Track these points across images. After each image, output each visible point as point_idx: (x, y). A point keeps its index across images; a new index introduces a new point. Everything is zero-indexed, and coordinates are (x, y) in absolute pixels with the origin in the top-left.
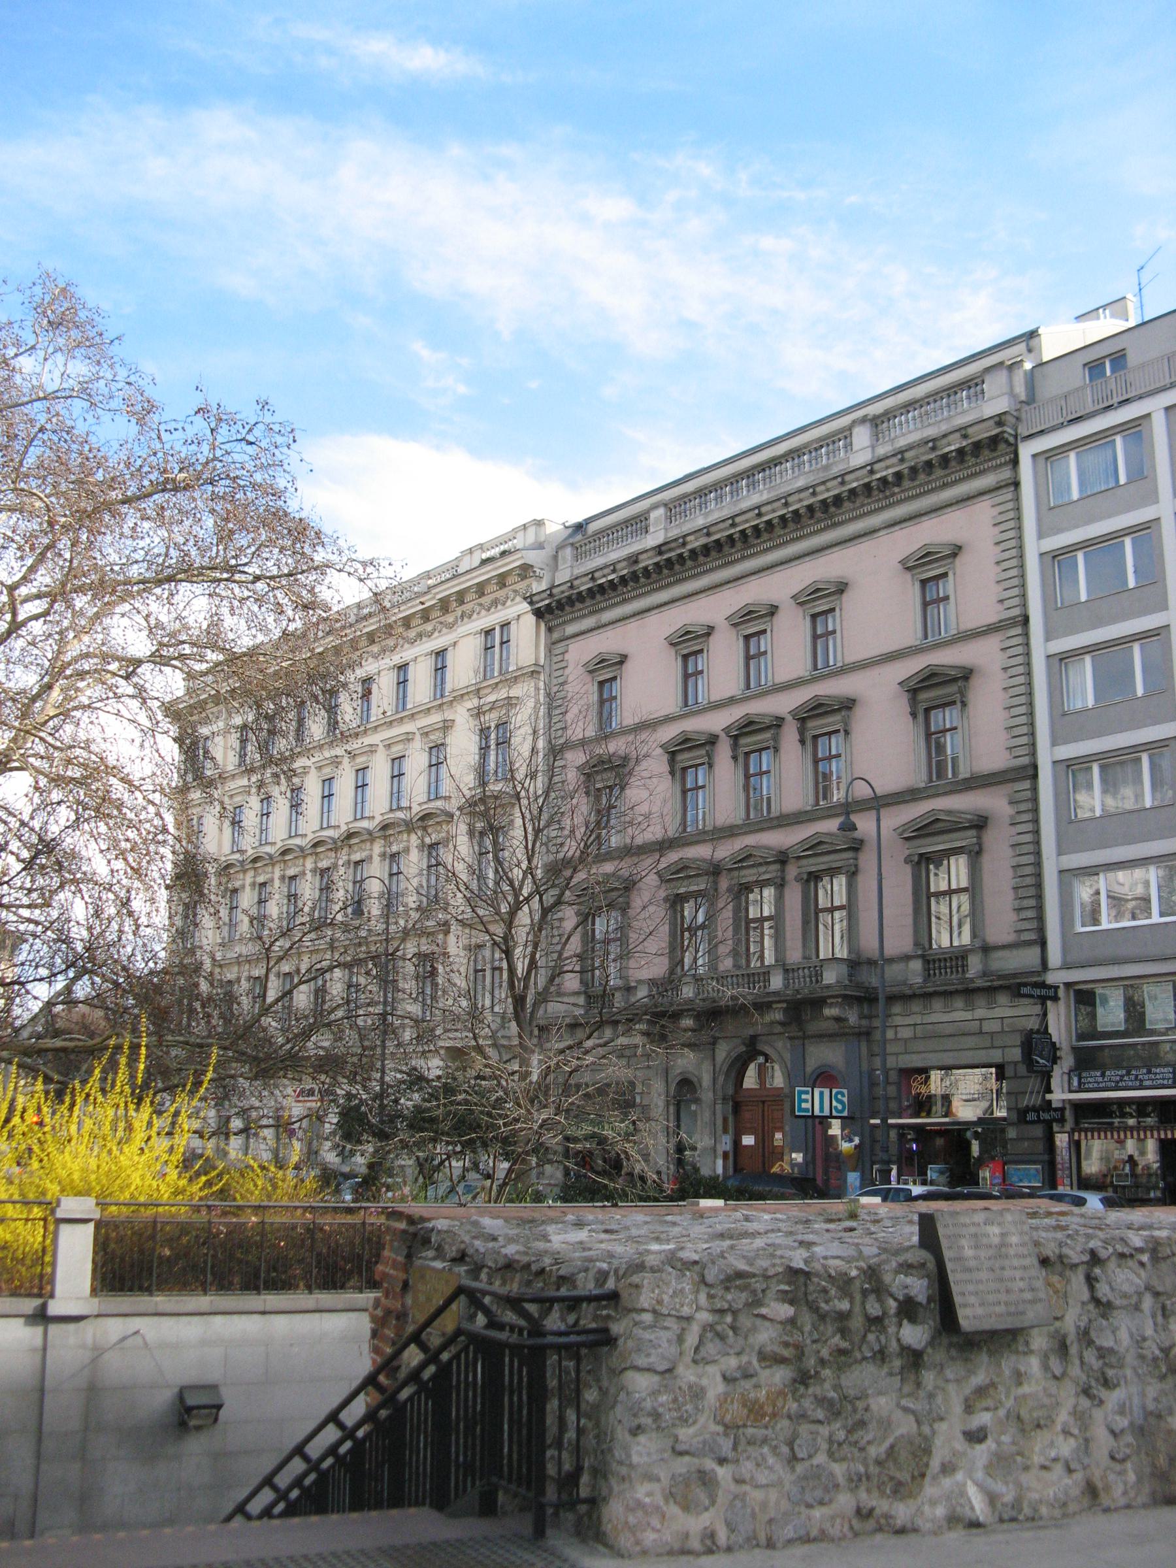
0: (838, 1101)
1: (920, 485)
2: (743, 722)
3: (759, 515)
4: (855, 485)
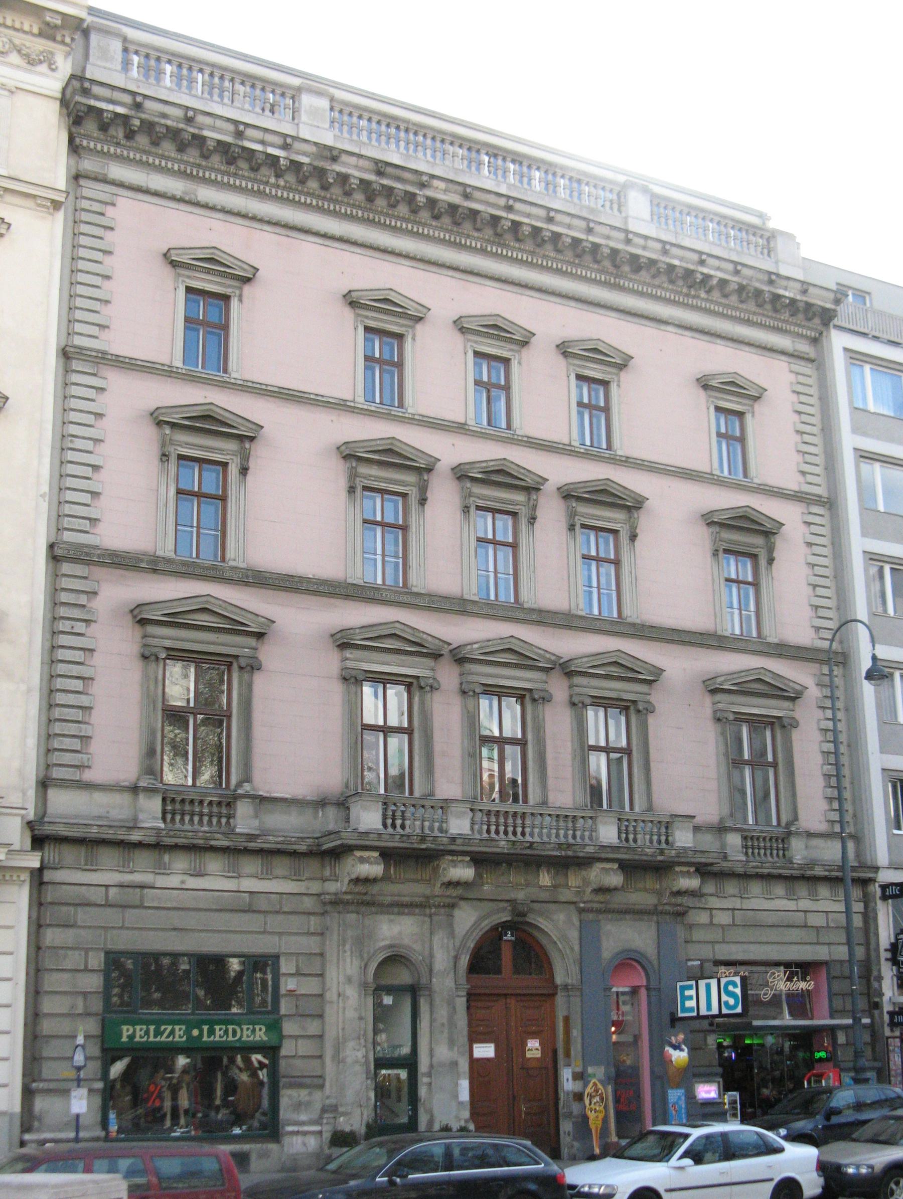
1: (746, 311)
2: (493, 466)
3: (550, 220)
4: (676, 262)
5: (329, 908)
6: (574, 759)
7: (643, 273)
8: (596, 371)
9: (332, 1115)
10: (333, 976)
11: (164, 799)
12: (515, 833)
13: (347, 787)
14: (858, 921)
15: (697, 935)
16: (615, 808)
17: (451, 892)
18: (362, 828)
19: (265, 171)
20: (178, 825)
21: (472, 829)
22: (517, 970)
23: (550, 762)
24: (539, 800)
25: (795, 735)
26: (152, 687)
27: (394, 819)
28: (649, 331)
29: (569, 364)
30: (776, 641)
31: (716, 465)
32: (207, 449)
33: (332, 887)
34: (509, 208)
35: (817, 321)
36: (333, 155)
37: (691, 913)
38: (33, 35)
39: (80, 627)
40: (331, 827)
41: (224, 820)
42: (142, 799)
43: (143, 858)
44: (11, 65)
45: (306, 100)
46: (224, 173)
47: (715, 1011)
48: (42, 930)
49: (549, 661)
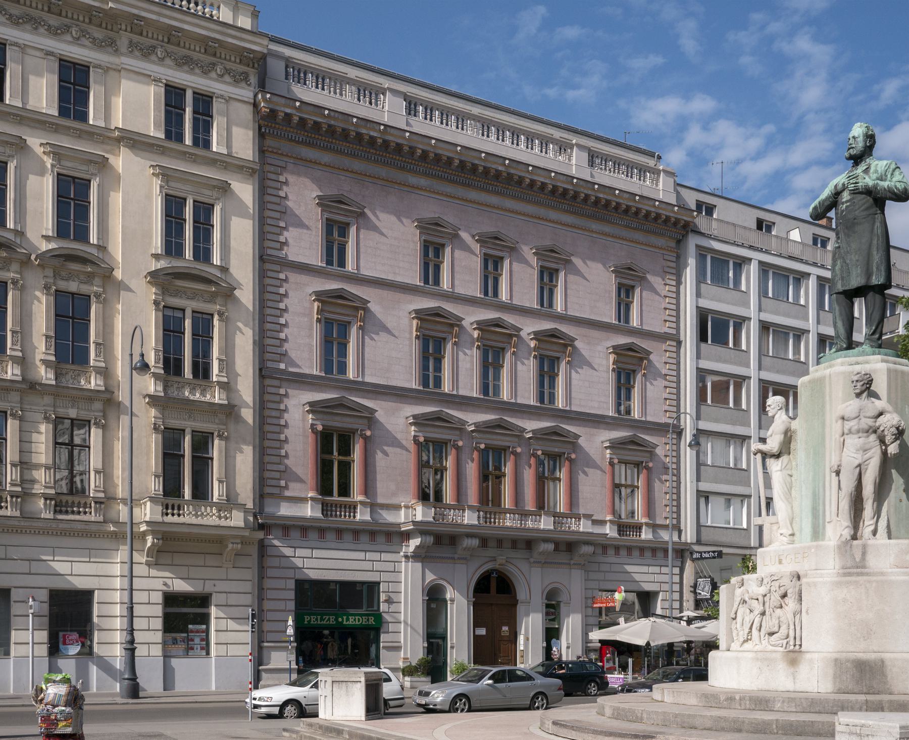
9: (151, 359)
22: (340, 495)
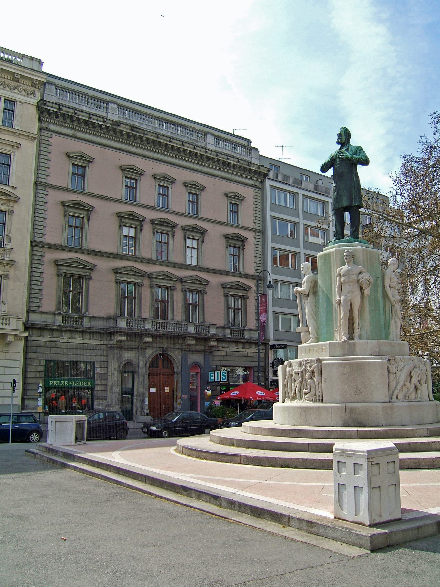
0: (223, 375)
1: (235, 171)
3: (183, 145)
4: (220, 159)
5: (110, 349)
6: (182, 307)
7: (210, 161)
8: (195, 190)
10: (111, 368)
11: (63, 317)
12: (164, 329)
13: (116, 314)
14: (262, 355)
15: (216, 358)
16: (194, 322)
17: (145, 345)
18: (120, 326)
19: (97, 128)
20: (67, 324)
21: (152, 327)
23: (175, 307)
24: (171, 318)
25: (248, 301)
26: (60, 284)
27: (129, 324)
28: (211, 179)
29: (186, 189)
30: (244, 273)
31: (229, 220)
32: (78, 212)
33: (111, 343)
34: (171, 142)
35: (262, 176)
36: (118, 124)
37: (214, 352)
38: (29, 86)
39: (39, 266)
40: (111, 325)
41: (80, 323)
42: (57, 317)
43: (56, 334)
44: (22, 95)
45: (110, 105)
46: (85, 128)
47: (219, 380)
48: (27, 354)
49: (176, 278)
